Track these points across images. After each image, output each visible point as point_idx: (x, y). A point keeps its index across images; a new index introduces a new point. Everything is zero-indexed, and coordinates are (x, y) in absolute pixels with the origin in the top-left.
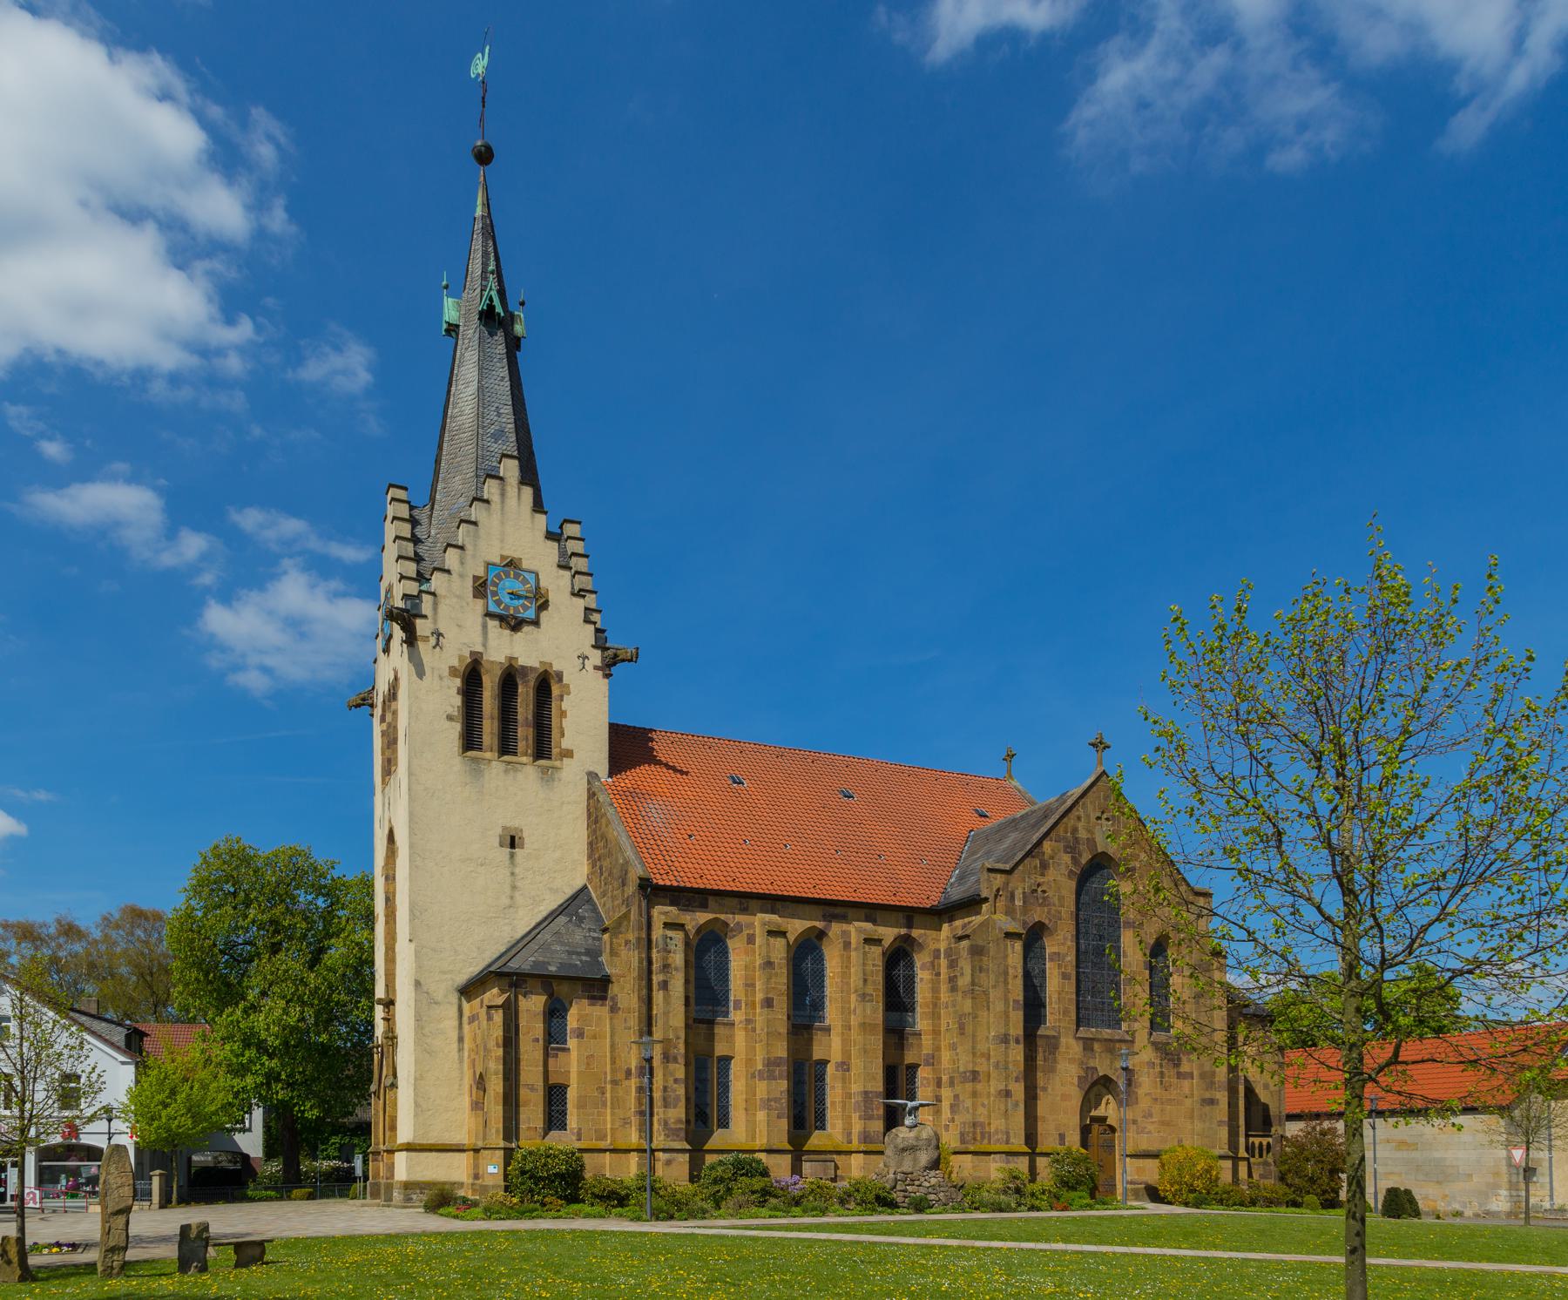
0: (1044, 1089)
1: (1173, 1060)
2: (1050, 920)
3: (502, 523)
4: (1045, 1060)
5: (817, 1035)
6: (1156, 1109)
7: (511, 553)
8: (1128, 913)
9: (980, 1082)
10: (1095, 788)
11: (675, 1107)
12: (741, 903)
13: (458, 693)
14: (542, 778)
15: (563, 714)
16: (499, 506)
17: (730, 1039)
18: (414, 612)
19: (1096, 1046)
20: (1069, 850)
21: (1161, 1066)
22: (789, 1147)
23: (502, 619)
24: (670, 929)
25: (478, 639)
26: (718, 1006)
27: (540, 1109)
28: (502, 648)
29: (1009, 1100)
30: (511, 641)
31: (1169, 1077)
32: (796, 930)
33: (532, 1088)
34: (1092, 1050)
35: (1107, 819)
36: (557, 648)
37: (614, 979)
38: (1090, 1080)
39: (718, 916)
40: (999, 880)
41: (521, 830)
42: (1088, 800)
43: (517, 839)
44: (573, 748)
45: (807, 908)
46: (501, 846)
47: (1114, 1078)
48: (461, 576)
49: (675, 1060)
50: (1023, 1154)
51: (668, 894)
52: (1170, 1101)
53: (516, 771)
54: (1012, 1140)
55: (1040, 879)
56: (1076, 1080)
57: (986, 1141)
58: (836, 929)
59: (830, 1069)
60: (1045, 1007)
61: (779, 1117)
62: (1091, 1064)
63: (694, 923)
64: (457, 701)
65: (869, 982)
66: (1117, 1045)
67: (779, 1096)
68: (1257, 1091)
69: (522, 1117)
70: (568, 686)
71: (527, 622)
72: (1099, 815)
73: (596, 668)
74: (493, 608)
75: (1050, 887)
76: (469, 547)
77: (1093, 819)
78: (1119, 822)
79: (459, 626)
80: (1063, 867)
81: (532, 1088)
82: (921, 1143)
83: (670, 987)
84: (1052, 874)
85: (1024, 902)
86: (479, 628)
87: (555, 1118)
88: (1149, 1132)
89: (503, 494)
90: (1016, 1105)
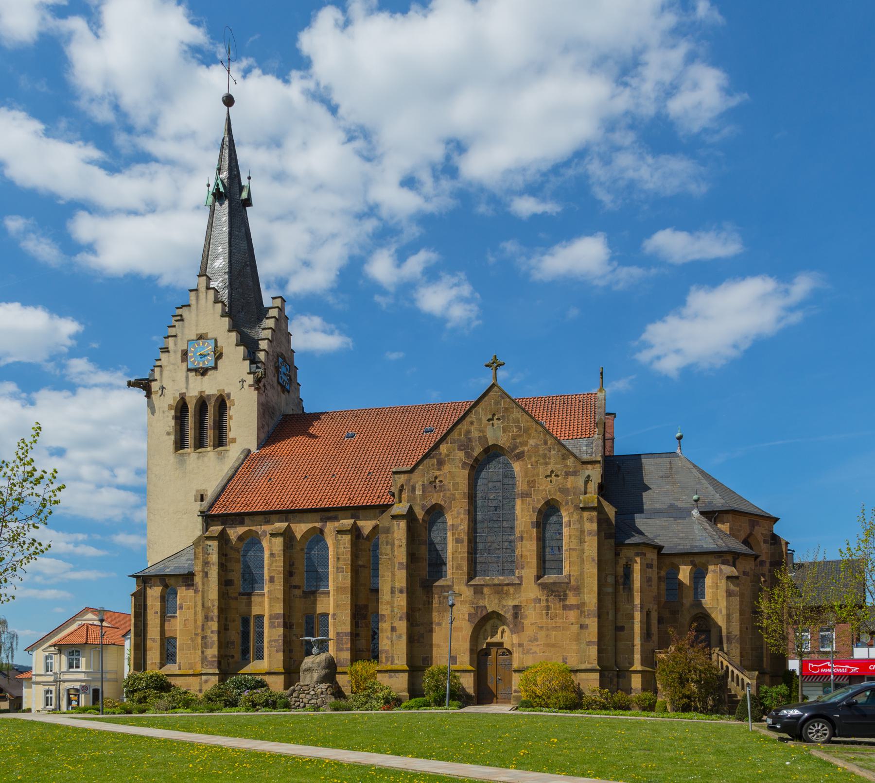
0: (439, 624)
1: (559, 596)
2: (445, 502)
3: (197, 315)
4: (440, 603)
5: (320, 597)
6: (542, 634)
7: (200, 332)
8: (521, 485)
9: (385, 622)
10: (486, 398)
11: (211, 648)
12: (266, 518)
13: (173, 419)
14: (218, 458)
15: (231, 418)
16: (195, 306)
17: (262, 604)
18: (151, 379)
19: (485, 590)
20: (462, 448)
21: (547, 601)
22: (598, 667)
23: (196, 370)
24: (209, 540)
25: (184, 385)
26: (320, 581)
27: (158, 652)
28: (197, 387)
29: (394, 633)
30: (202, 382)
31: (555, 609)
32: (302, 530)
33: (154, 640)
34: (482, 593)
35: (498, 419)
36: (228, 379)
37: (196, 574)
38: (479, 616)
39: (251, 528)
40: (402, 479)
41: (207, 491)
42: (479, 408)
43: (204, 496)
44: (236, 437)
45: (310, 515)
46: (196, 501)
47: (502, 613)
48: (175, 352)
49: (212, 619)
50: (403, 671)
51: (220, 518)
52: (555, 628)
53: (204, 456)
54: (396, 662)
55: (437, 473)
56: (467, 617)
57: (389, 663)
58: (330, 528)
59: (330, 617)
60: (445, 564)
61: (277, 651)
62: (481, 603)
63: (235, 534)
64: (172, 423)
65: (341, 559)
66: (505, 588)
67: (277, 638)
68: (713, 616)
69: (149, 657)
70: (233, 400)
71: (210, 369)
72: (490, 417)
73: (250, 386)
74: (190, 366)
75: (446, 477)
76: (179, 335)
77: (484, 421)
78: (508, 419)
79: (173, 381)
80: (457, 461)
81: (154, 640)
82: (314, 665)
83: (209, 576)
84: (447, 468)
85: (423, 491)
86: (184, 379)
87: (168, 656)
88: (535, 653)
89: (197, 298)
90: (400, 636)
